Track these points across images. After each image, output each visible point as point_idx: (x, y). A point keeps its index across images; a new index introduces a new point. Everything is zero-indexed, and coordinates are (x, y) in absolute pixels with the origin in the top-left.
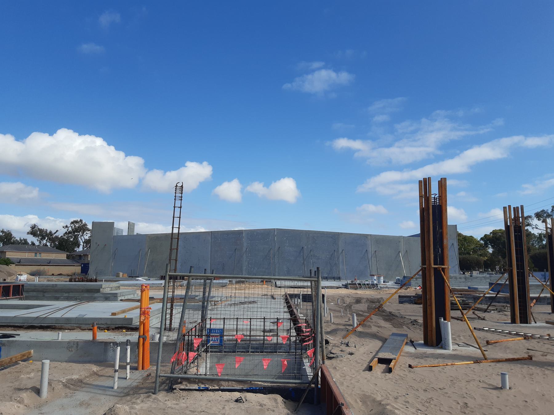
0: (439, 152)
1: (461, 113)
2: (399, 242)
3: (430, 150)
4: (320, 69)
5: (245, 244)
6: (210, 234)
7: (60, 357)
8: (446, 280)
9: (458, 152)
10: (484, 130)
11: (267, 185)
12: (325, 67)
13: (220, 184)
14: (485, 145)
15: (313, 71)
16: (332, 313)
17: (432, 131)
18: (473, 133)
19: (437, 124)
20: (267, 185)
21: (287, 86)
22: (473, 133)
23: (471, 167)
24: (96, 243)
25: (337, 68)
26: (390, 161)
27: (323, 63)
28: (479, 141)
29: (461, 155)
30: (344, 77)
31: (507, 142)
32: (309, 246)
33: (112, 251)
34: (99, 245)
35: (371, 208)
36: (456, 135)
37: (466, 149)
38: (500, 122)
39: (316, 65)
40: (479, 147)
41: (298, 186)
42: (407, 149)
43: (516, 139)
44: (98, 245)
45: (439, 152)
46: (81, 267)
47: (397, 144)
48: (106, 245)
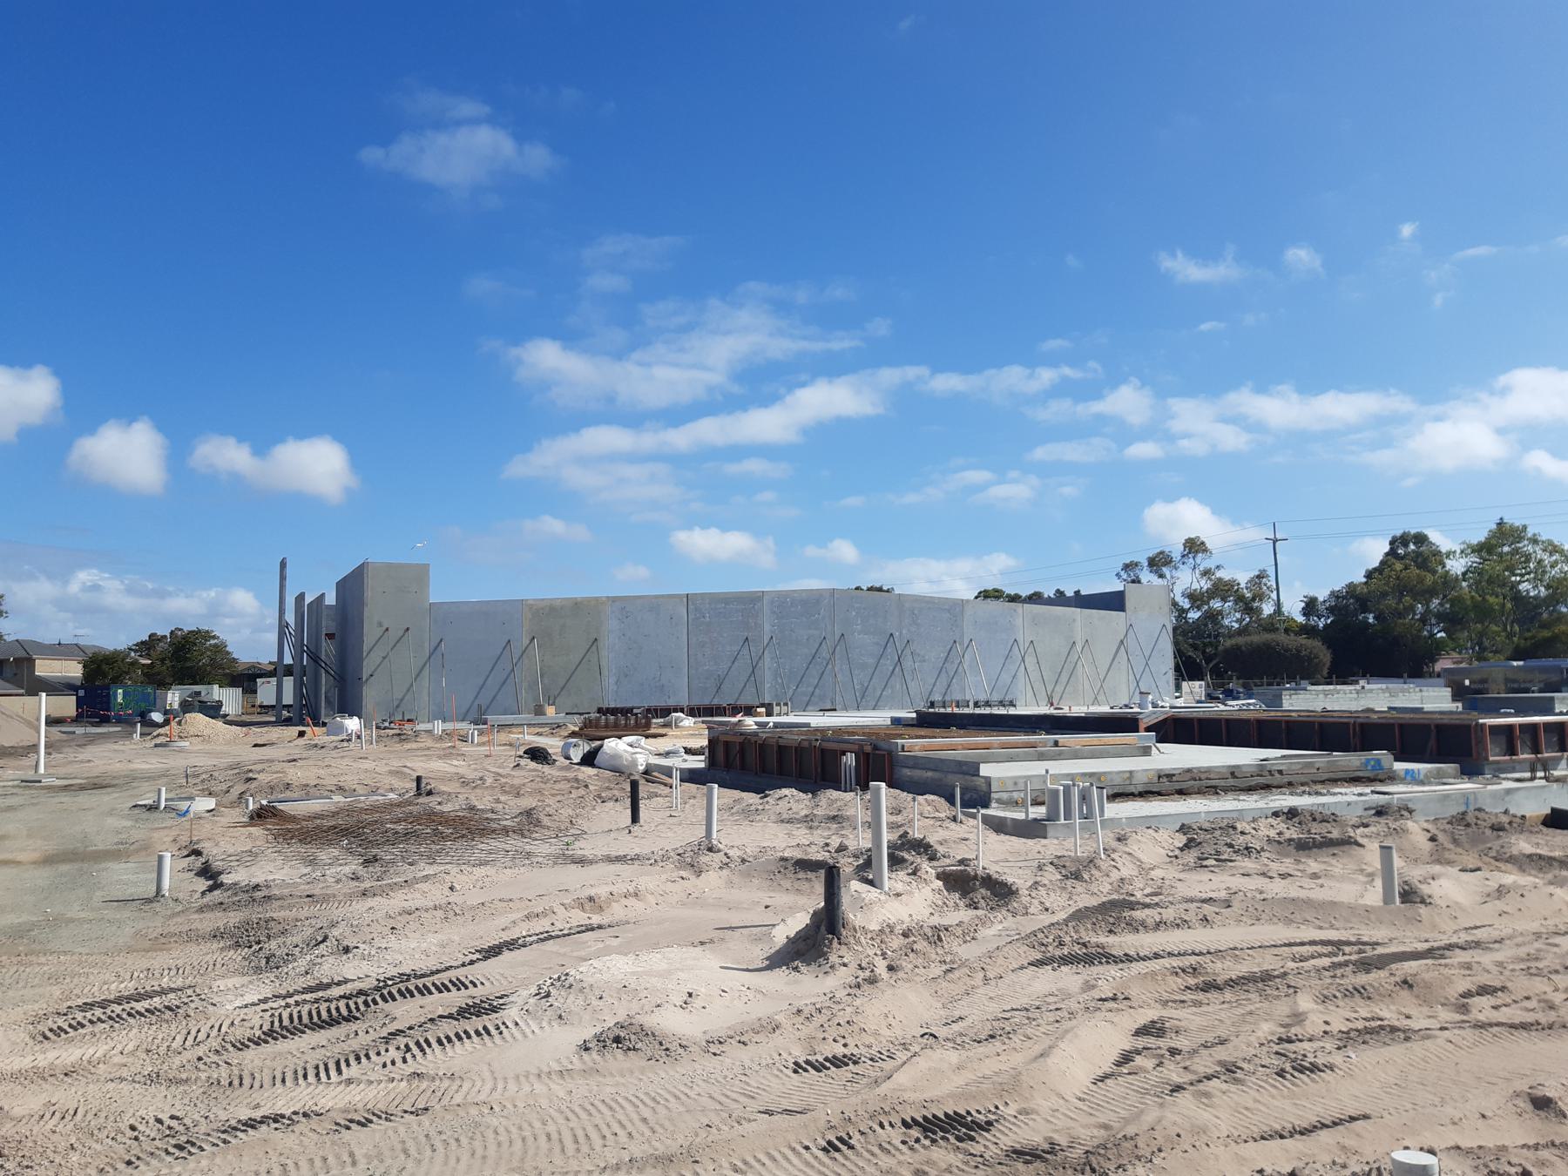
0: (736, 389)
1: (802, 296)
2: (1074, 620)
3: (715, 378)
4: (475, 122)
5: (767, 627)
6: (685, 599)
7: (451, 888)
8: (817, 720)
9: (782, 390)
10: (841, 343)
11: (261, 449)
12: (490, 121)
13: (91, 429)
14: (843, 379)
15: (459, 123)
16: (168, 855)
17: (728, 332)
18: (818, 346)
19: (744, 317)
20: (261, 449)
21: (371, 155)
22: (818, 346)
23: (805, 431)
24: (380, 625)
25: (522, 130)
26: (611, 399)
27: (486, 110)
28: (830, 368)
29: (789, 399)
30: (539, 158)
31: (890, 376)
32: (904, 632)
33: (427, 645)
34: (387, 629)
35: (554, 525)
36: (782, 347)
37: (803, 385)
38: (881, 327)
39: (468, 108)
40: (830, 382)
41: (356, 460)
42: (662, 373)
43: (912, 372)
44: (384, 628)
45: (736, 389)
46: (75, 697)
47: (636, 356)
48: (408, 629)
